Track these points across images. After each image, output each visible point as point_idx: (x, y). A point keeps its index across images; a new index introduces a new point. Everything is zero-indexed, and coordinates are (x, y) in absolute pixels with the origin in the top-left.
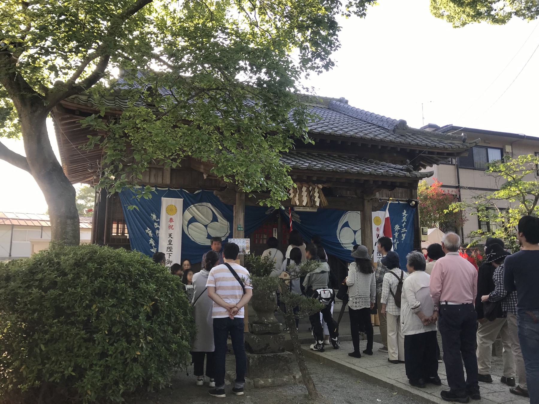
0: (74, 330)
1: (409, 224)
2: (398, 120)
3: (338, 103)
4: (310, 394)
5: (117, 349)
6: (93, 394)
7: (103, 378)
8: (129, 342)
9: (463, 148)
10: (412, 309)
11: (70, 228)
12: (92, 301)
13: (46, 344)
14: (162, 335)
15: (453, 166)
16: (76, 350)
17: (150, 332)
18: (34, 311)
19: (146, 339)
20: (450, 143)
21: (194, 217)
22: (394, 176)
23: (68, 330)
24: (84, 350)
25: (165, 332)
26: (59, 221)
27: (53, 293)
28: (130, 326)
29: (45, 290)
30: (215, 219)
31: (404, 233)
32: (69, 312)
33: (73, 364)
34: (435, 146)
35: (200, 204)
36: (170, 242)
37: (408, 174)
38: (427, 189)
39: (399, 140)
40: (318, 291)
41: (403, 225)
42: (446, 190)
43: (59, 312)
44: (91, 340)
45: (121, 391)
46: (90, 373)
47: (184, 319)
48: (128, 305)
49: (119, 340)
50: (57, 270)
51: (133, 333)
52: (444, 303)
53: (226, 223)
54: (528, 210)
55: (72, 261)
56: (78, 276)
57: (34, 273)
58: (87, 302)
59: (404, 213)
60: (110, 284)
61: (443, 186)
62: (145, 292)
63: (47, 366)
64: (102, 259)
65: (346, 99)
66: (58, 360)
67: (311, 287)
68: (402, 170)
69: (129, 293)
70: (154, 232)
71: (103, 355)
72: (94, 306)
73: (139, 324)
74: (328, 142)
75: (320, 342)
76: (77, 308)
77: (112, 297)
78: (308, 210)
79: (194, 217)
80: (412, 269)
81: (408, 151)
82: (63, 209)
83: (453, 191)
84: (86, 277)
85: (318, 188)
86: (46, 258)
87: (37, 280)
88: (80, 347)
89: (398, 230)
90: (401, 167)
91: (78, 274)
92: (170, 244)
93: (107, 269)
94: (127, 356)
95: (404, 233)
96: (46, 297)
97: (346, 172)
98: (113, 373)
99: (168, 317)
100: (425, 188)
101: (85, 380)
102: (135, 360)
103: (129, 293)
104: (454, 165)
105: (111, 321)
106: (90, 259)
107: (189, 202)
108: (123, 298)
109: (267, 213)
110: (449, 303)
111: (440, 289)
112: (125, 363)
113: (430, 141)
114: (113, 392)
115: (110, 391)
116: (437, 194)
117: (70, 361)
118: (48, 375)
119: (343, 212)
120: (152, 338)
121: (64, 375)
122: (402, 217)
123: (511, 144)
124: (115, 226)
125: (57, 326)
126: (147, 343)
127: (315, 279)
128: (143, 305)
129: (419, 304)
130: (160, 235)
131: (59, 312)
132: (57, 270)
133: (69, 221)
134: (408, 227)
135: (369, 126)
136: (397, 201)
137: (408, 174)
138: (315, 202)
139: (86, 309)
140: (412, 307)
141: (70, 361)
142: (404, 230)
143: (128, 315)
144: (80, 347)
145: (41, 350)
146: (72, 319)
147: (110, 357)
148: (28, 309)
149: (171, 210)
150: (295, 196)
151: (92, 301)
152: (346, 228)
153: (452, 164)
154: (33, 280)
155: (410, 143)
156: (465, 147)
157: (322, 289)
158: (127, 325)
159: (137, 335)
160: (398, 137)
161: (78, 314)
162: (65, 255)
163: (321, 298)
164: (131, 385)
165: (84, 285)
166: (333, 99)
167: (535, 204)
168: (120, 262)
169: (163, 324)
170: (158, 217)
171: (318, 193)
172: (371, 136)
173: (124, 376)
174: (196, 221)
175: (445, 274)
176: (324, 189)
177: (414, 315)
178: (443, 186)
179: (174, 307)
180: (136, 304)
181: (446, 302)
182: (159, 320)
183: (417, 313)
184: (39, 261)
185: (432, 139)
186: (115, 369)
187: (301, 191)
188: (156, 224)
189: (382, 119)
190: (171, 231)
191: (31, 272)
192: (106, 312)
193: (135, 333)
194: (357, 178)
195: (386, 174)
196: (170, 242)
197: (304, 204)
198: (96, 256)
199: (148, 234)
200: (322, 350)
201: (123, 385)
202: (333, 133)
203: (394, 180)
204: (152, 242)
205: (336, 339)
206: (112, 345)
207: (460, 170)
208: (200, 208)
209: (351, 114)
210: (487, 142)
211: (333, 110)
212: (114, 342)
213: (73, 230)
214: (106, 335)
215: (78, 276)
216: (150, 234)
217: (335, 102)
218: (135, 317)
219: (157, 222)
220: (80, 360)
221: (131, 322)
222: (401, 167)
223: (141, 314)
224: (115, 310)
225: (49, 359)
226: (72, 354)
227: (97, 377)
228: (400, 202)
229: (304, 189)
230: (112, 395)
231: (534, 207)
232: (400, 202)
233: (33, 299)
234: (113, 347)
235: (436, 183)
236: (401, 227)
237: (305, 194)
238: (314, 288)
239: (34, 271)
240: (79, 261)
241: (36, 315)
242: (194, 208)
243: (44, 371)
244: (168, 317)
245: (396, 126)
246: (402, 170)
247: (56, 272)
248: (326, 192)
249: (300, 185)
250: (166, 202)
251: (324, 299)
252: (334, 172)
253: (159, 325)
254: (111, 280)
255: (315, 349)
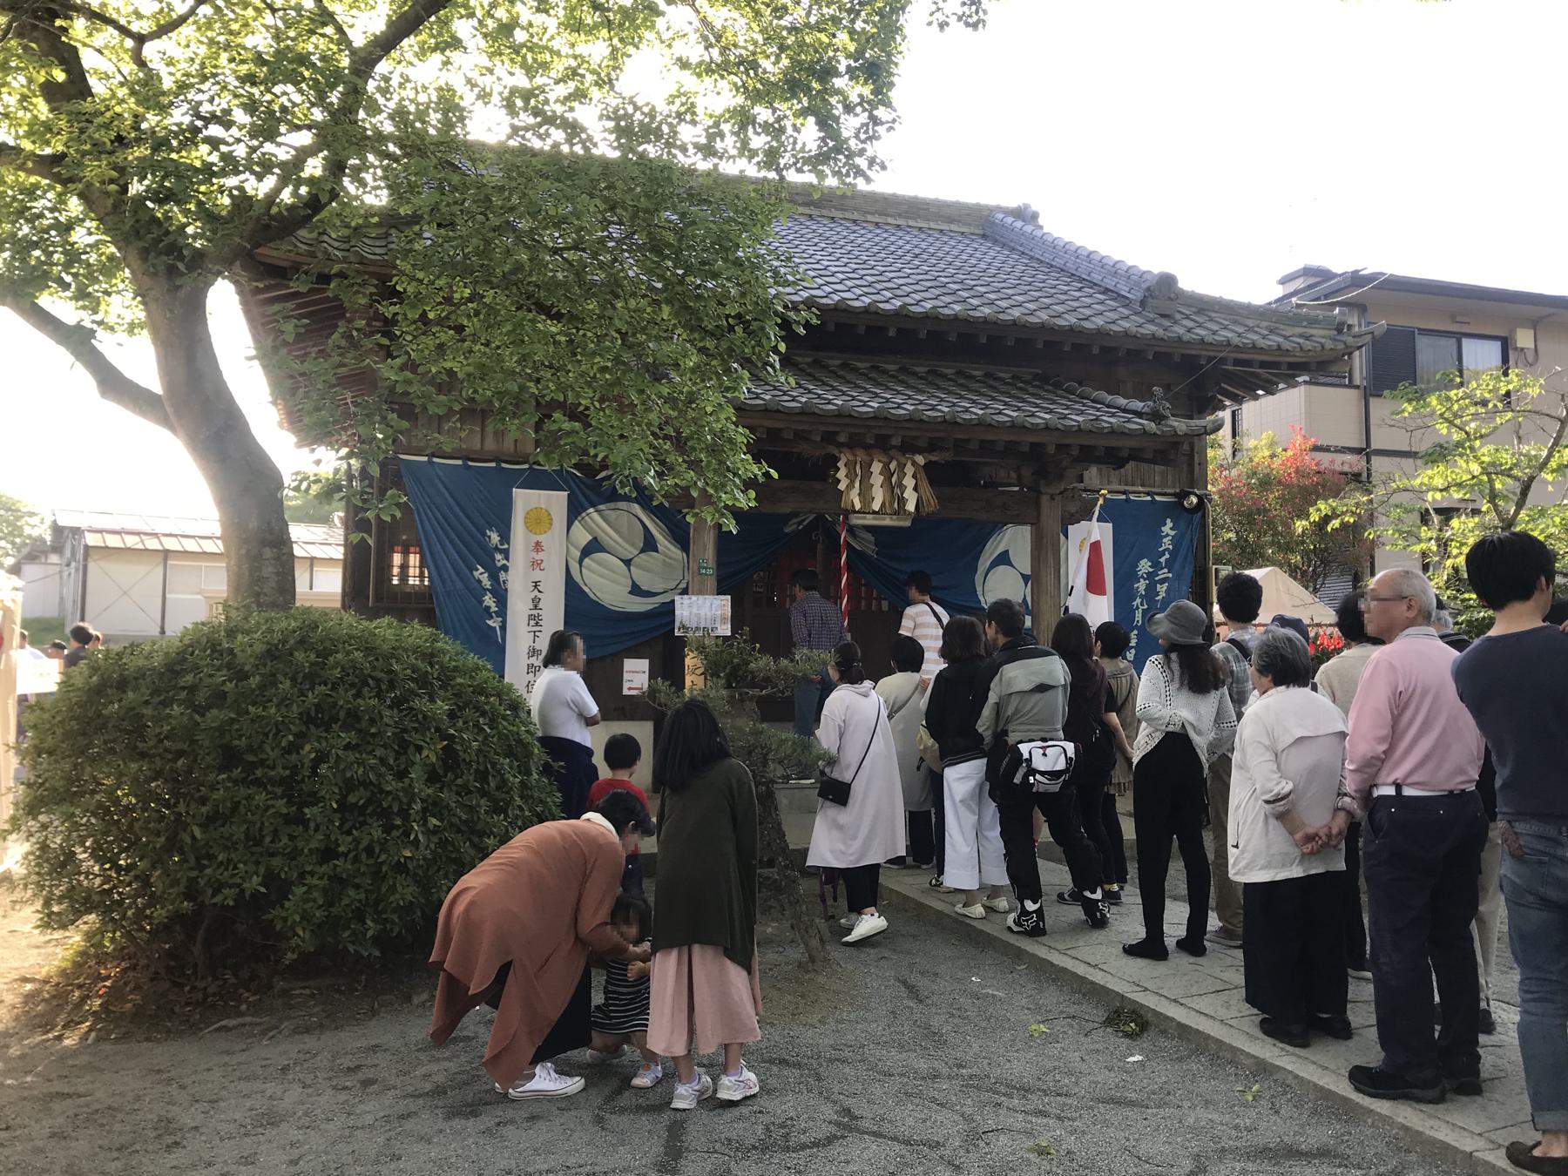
0: (261, 798)
1: (1180, 559)
2: (1156, 271)
3: (1010, 220)
4: (812, 959)
5: (357, 841)
6: (307, 935)
7: (330, 904)
8: (388, 829)
9: (1383, 337)
10: (1267, 802)
11: (270, 569)
12: (301, 736)
13: (204, 826)
14: (464, 817)
15: (1352, 393)
16: (268, 839)
17: (434, 807)
18: (180, 754)
19: (426, 821)
20: (1301, 336)
21: (595, 538)
22: (1113, 432)
23: (249, 798)
24: (285, 840)
25: (472, 809)
26: (243, 552)
27: (216, 716)
28: (389, 793)
29: (202, 710)
30: (650, 545)
31: (1162, 581)
32: (251, 758)
33: (262, 870)
34: (1254, 346)
35: (612, 505)
36: (536, 603)
37: (1151, 426)
38: (1273, 456)
39: (1150, 329)
40: (1024, 748)
41: (1163, 560)
42: (1325, 459)
43: (230, 757)
44: (301, 820)
45: (370, 934)
46: (299, 890)
47: (522, 782)
48: (385, 746)
49: (364, 823)
50: (229, 666)
51: (395, 810)
52: (1391, 791)
53: (676, 552)
54: (1502, 520)
55: (259, 648)
56: (271, 681)
57: (178, 673)
58: (291, 738)
59: (1168, 528)
60: (344, 698)
61: (1316, 448)
62: (425, 717)
63: (208, 871)
64: (328, 644)
65: (1034, 208)
66: (229, 861)
67: (1005, 733)
68: (1139, 414)
69: (386, 720)
70: (494, 577)
71: (328, 853)
72: (308, 747)
73: (408, 791)
74: (952, 338)
75: (1030, 906)
76: (269, 750)
77: (346, 727)
78: (887, 522)
79: (595, 538)
80: (1266, 681)
81: (1177, 359)
82: (253, 524)
83: (1352, 462)
84: (288, 683)
85: (914, 463)
86: (204, 640)
87: (183, 688)
88: (275, 833)
89: (1149, 574)
90: (1138, 405)
91: (274, 675)
92: (536, 607)
93: (337, 664)
94: (383, 857)
95: (1162, 581)
96: (203, 726)
97: (981, 424)
98: (352, 892)
99: (482, 776)
100: (1267, 453)
101: (287, 904)
102: (400, 868)
103: (386, 720)
104: (1358, 387)
105: (346, 780)
106: (302, 642)
107: (582, 499)
108: (373, 730)
109: (787, 530)
110: (1408, 792)
111: (1384, 747)
112: (377, 875)
113: (1241, 330)
114: (354, 934)
115: (347, 934)
116: (1297, 471)
117: (257, 863)
118: (210, 892)
119: (996, 526)
120: (442, 820)
121: (242, 891)
122: (1159, 538)
123: (1534, 324)
124: (397, 559)
125: (227, 789)
126: (430, 832)
127: (1017, 711)
128: (419, 749)
129: (1289, 787)
130: (509, 586)
131: (230, 757)
132: (229, 666)
133: (268, 553)
134: (1177, 566)
135: (1080, 290)
136: (1148, 494)
137: (1151, 426)
138: (902, 501)
139: (289, 752)
140: (1267, 797)
141: (257, 863)
142: (1164, 573)
143: (383, 769)
144: (275, 833)
145: (193, 837)
146: (259, 773)
147: (342, 860)
148: (166, 750)
149: (538, 520)
150: (850, 486)
151: (301, 736)
152: (1002, 568)
153: (1351, 386)
154: (174, 688)
155: (1180, 338)
156: (1341, 346)
157: (1040, 744)
158: (381, 791)
159: (405, 814)
160: (1152, 321)
161: (270, 762)
162: (248, 632)
163: (1033, 772)
164: (393, 923)
165: (283, 700)
166: (999, 209)
167: (1520, 505)
168: (369, 650)
169: (470, 792)
170: (505, 537)
171: (914, 476)
172: (1071, 319)
173: (377, 902)
174: (602, 549)
175: (1404, 698)
176: (928, 467)
177: (1272, 821)
178: (1316, 448)
179: (496, 753)
180: (403, 746)
181: (1398, 787)
182: (459, 781)
183: (1281, 817)
184: (190, 646)
185: (1250, 323)
186: (357, 887)
187: (867, 474)
188: (498, 557)
189: (1114, 269)
190: (537, 575)
191: (172, 671)
192: (332, 761)
193: (400, 810)
194: (1012, 438)
195: (1089, 426)
196: (536, 603)
197: (876, 506)
198: (314, 637)
199: (480, 582)
200: (1037, 932)
201: (373, 920)
202: (963, 315)
203: (1114, 443)
204: (489, 601)
205: (1098, 895)
206: (349, 833)
207: (1373, 401)
208: (612, 515)
209: (1037, 254)
210: (1459, 319)
211: (995, 242)
212: (353, 827)
213: (277, 574)
214: (335, 811)
215: (271, 681)
216: (487, 583)
217: (1000, 216)
218: (402, 775)
219: (501, 551)
220: (276, 862)
221: (391, 784)
222: (1138, 405)
223: (416, 767)
224: (352, 756)
225: (212, 857)
226: (260, 849)
227: (314, 901)
228: (1158, 498)
229: (876, 467)
230: (353, 943)
231: (1517, 512)
232: (1158, 498)
233: (173, 729)
234: (350, 839)
235: (1299, 439)
236: (1156, 565)
237: (877, 479)
238: (1011, 739)
239: (178, 668)
240: (276, 646)
241: (180, 763)
242: (596, 516)
243: (202, 882)
244: (482, 776)
245: (1148, 289)
246: (1139, 414)
247: (224, 672)
248: (933, 475)
249: (866, 458)
250: (524, 500)
251: (1042, 773)
252: (949, 423)
253: (458, 793)
254: (347, 691)
255: (1016, 929)
